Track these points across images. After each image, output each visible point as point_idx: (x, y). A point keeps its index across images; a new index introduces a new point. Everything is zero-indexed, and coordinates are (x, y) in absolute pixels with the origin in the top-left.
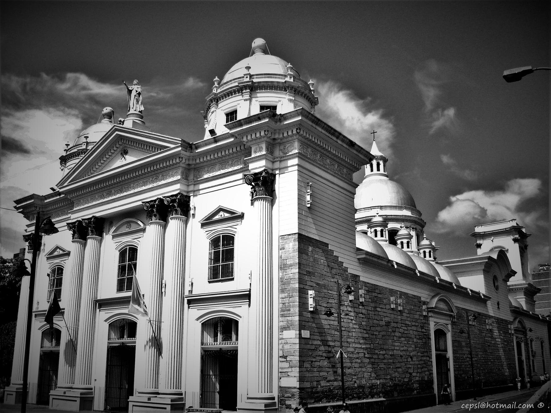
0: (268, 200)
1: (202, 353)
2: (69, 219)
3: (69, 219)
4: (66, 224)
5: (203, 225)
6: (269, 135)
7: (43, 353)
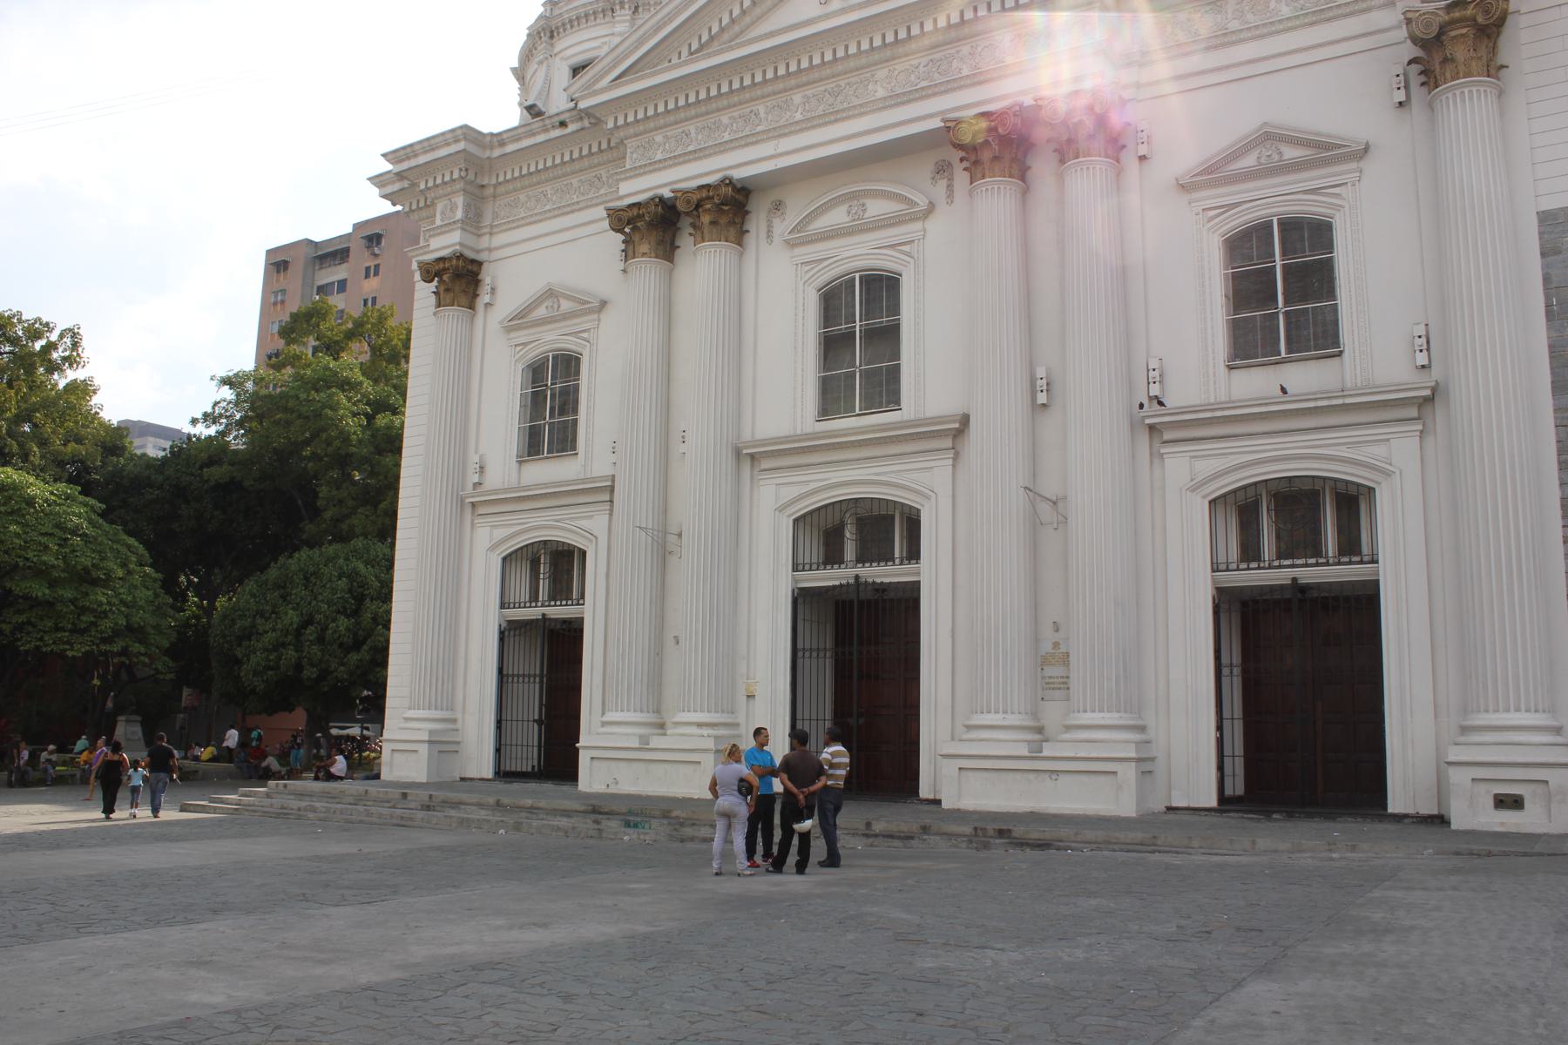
0: (1088, 168)
1: (500, 625)
2: (426, 250)
3: (426, 250)
4: (604, 214)
5: (509, 330)
6: (471, 176)
7: (509, 622)
